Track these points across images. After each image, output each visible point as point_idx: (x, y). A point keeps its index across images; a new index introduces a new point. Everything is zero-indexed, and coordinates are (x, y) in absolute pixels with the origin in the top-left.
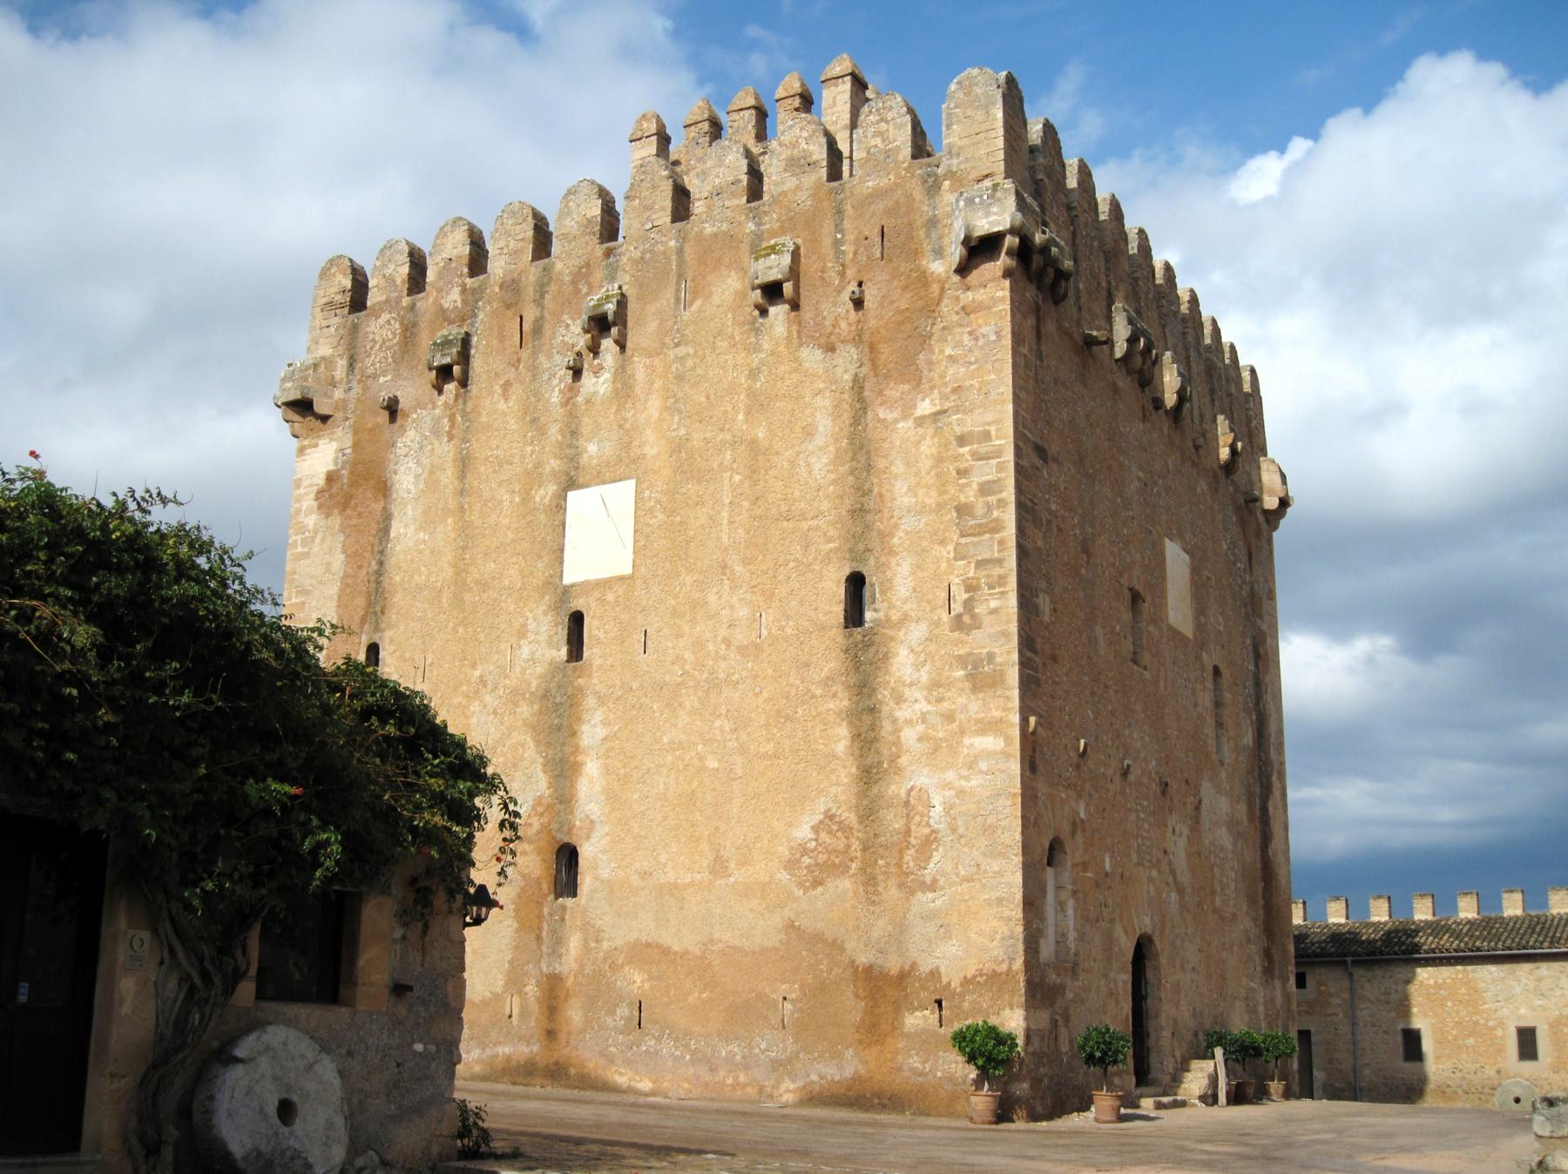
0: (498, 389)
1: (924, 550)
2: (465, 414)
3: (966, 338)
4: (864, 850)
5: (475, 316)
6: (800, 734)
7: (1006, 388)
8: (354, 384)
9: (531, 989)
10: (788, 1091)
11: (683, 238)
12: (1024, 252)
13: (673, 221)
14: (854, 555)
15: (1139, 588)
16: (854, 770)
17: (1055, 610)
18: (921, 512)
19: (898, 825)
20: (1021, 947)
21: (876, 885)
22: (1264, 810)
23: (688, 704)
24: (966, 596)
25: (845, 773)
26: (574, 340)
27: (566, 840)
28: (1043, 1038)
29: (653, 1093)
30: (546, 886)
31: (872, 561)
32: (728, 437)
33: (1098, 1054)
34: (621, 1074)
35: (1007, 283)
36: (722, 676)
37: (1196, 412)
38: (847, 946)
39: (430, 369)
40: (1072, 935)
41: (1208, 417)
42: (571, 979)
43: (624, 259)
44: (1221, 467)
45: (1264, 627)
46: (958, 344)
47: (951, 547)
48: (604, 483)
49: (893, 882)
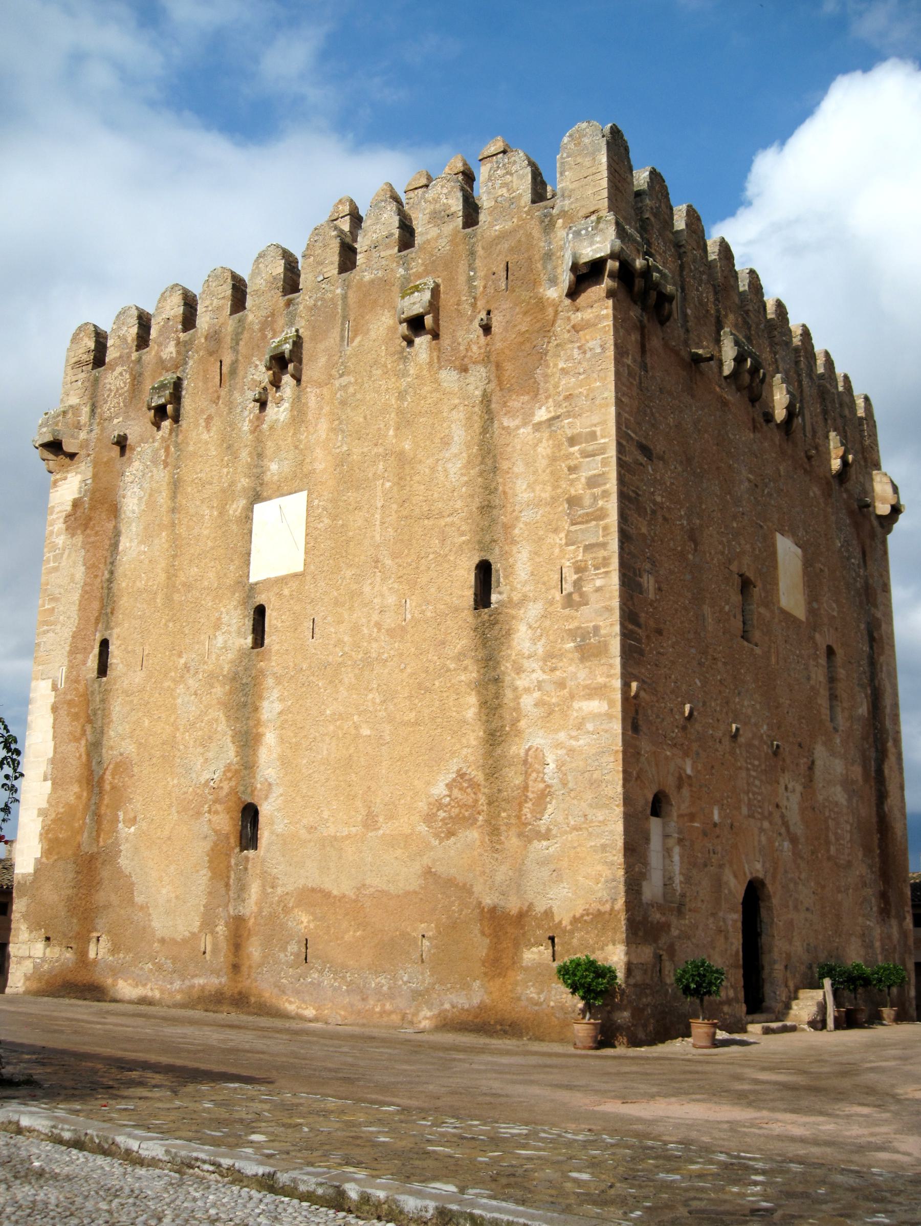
0: (202, 422)
1: (541, 539)
2: (177, 445)
3: (576, 351)
4: (490, 804)
5: (186, 363)
6: (437, 703)
7: (610, 393)
8: (95, 427)
9: (221, 929)
10: (426, 1018)
11: (347, 286)
12: (625, 274)
13: (340, 273)
14: (484, 546)
15: (750, 575)
16: (481, 733)
17: (660, 589)
18: (538, 506)
19: (518, 781)
20: (622, 888)
21: (499, 835)
22: (880, 772)
23: (346, 680)
24: (576, 577)
25: (474, 736)
26: (262, 378)
27: (249, 801)
28: (645, 972)
29: (316, 1019)
30: (233, 840)
31: (497, 550)
32: (381, 450)
33: (693, 986)
34: (290, 1003)
35: (610, 302)
36: (374, 655)
37: (808, 428)
38: (475, 889)
39: (149, 409)
40: (678, 879)
41: (820, 433)
42: (252, 921)
43: (301, 307)
44: (834, 476)
45: (879, 615)
46: (570, 358)
47: (562, 535)
48: (283, 495)
49: (513, 832)
